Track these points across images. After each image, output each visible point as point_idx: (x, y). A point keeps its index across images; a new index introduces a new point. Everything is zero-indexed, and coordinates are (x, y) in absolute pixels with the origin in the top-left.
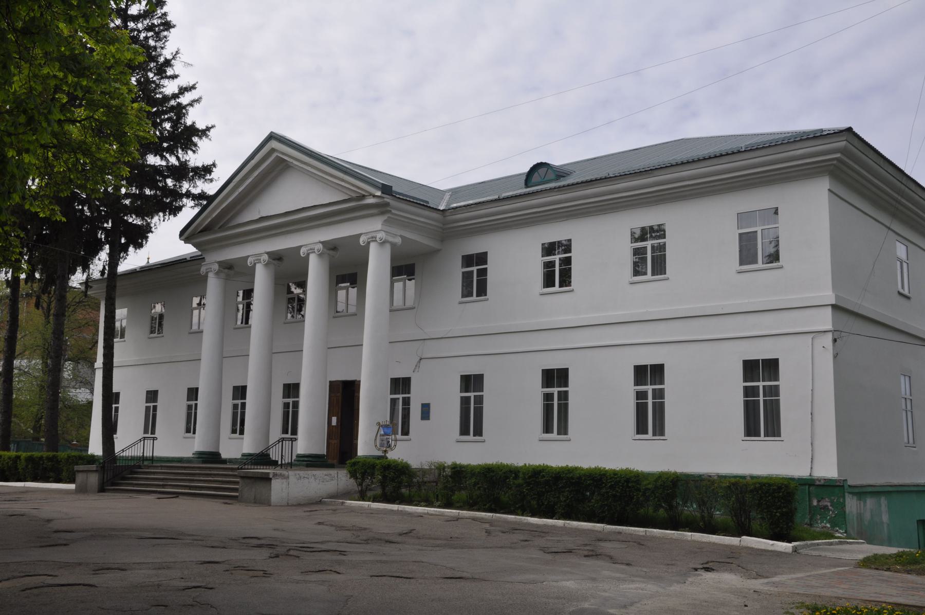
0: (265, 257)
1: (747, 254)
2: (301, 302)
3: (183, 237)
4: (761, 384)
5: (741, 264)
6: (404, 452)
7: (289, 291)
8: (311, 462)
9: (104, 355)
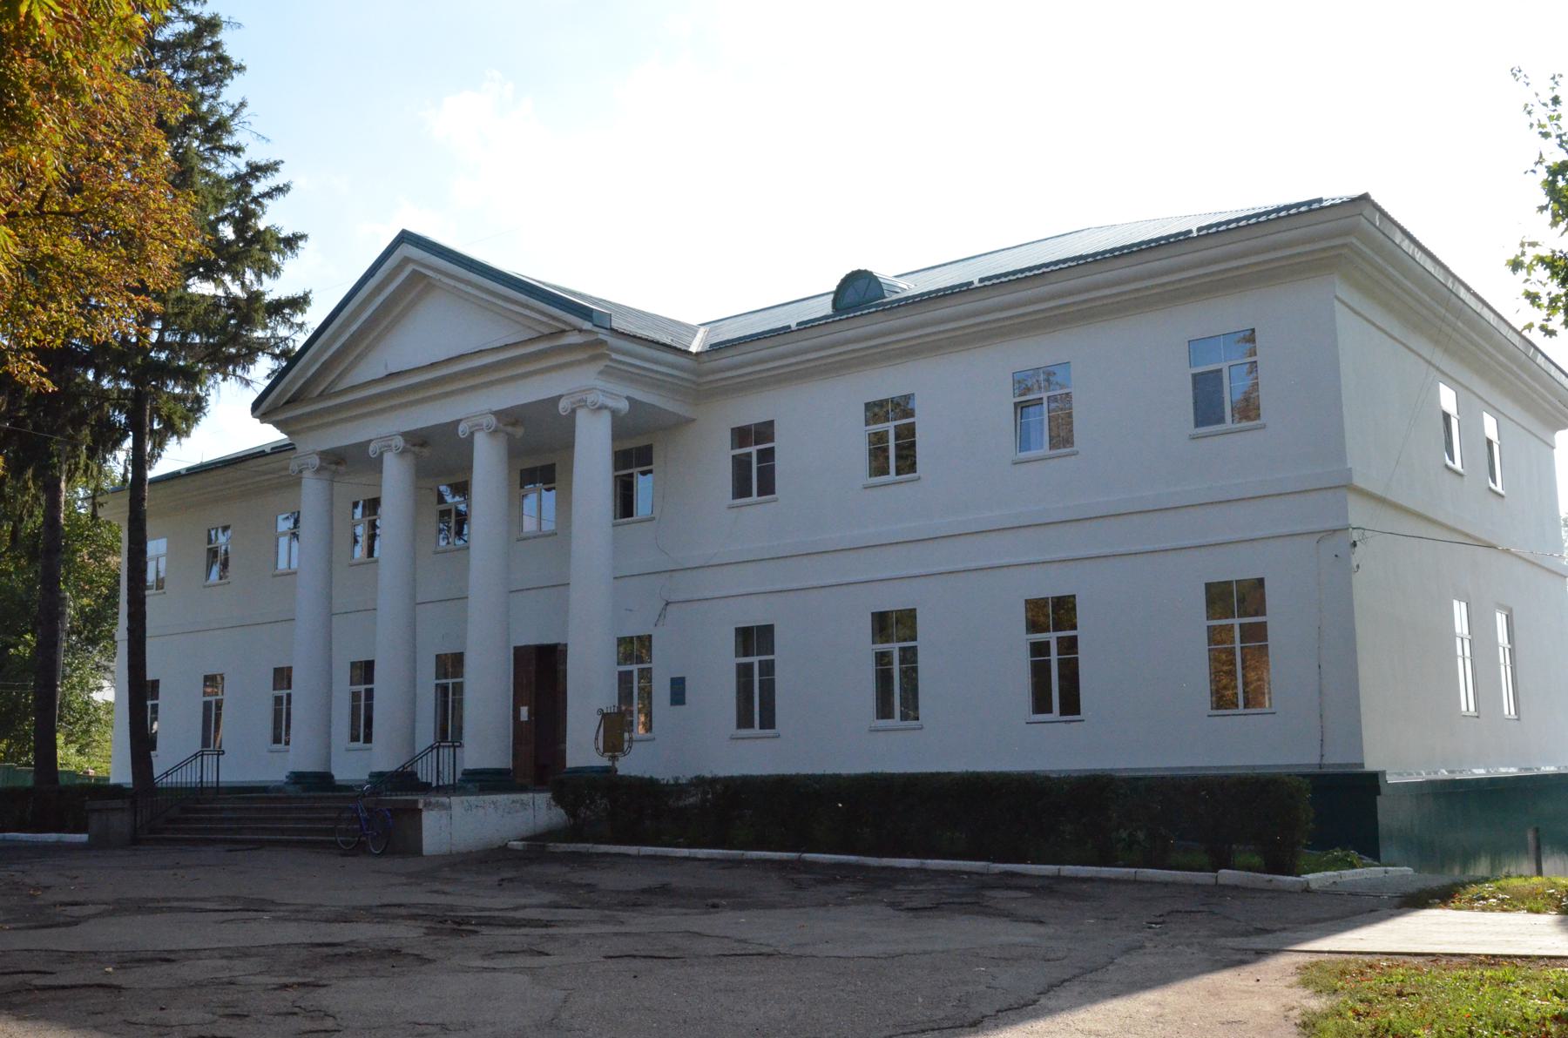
0: (400, 442)
1: (1207, 408)
2: (462, 519)
3: (258, 412)
4: (1236, 622)
5: (1197, 425)
6: (641, 761)
7: (441, 499)
8: (485, 781)
9: (130, 616)
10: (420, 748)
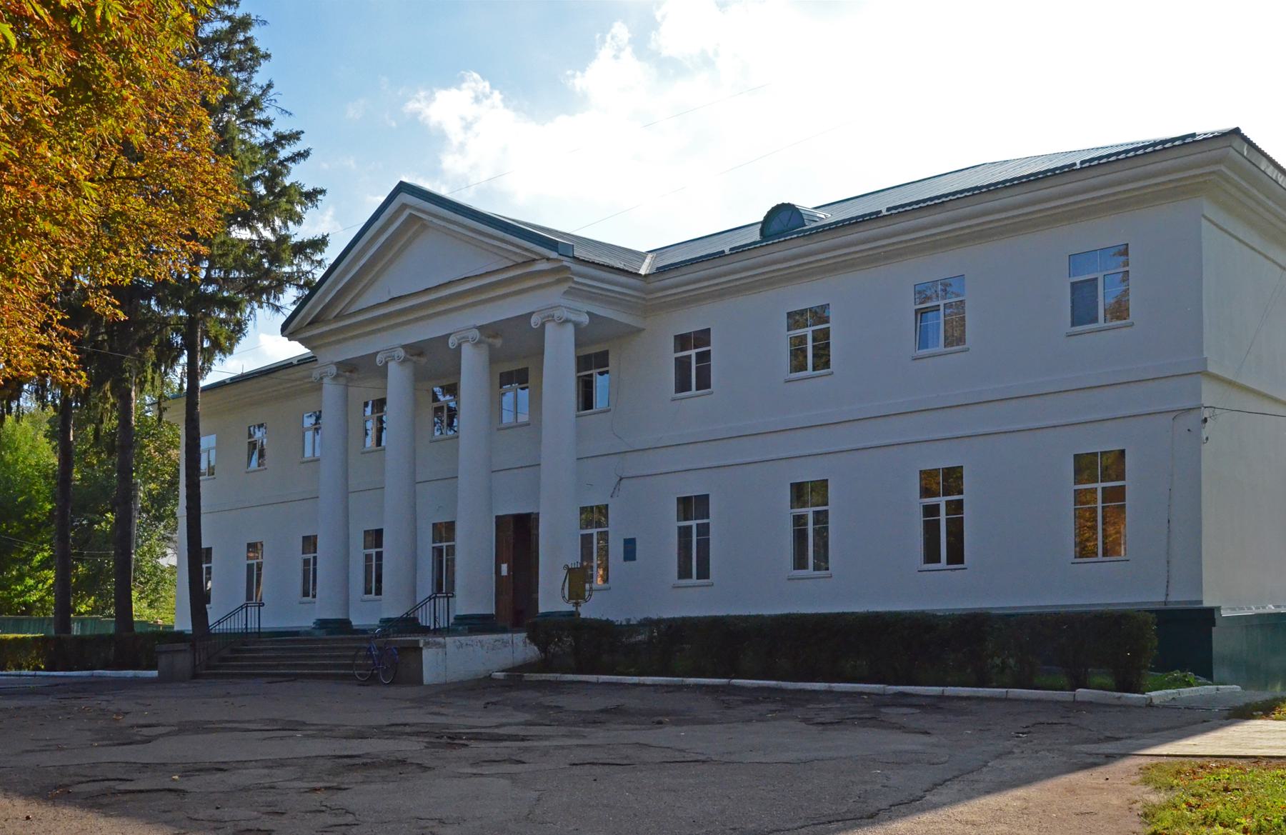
2: (452, 413)
3: (287, 332)
4: (1099, 486)
7: (435, 399)
8: (474, 625)
9: (188, 497)
10: (419, 600)
